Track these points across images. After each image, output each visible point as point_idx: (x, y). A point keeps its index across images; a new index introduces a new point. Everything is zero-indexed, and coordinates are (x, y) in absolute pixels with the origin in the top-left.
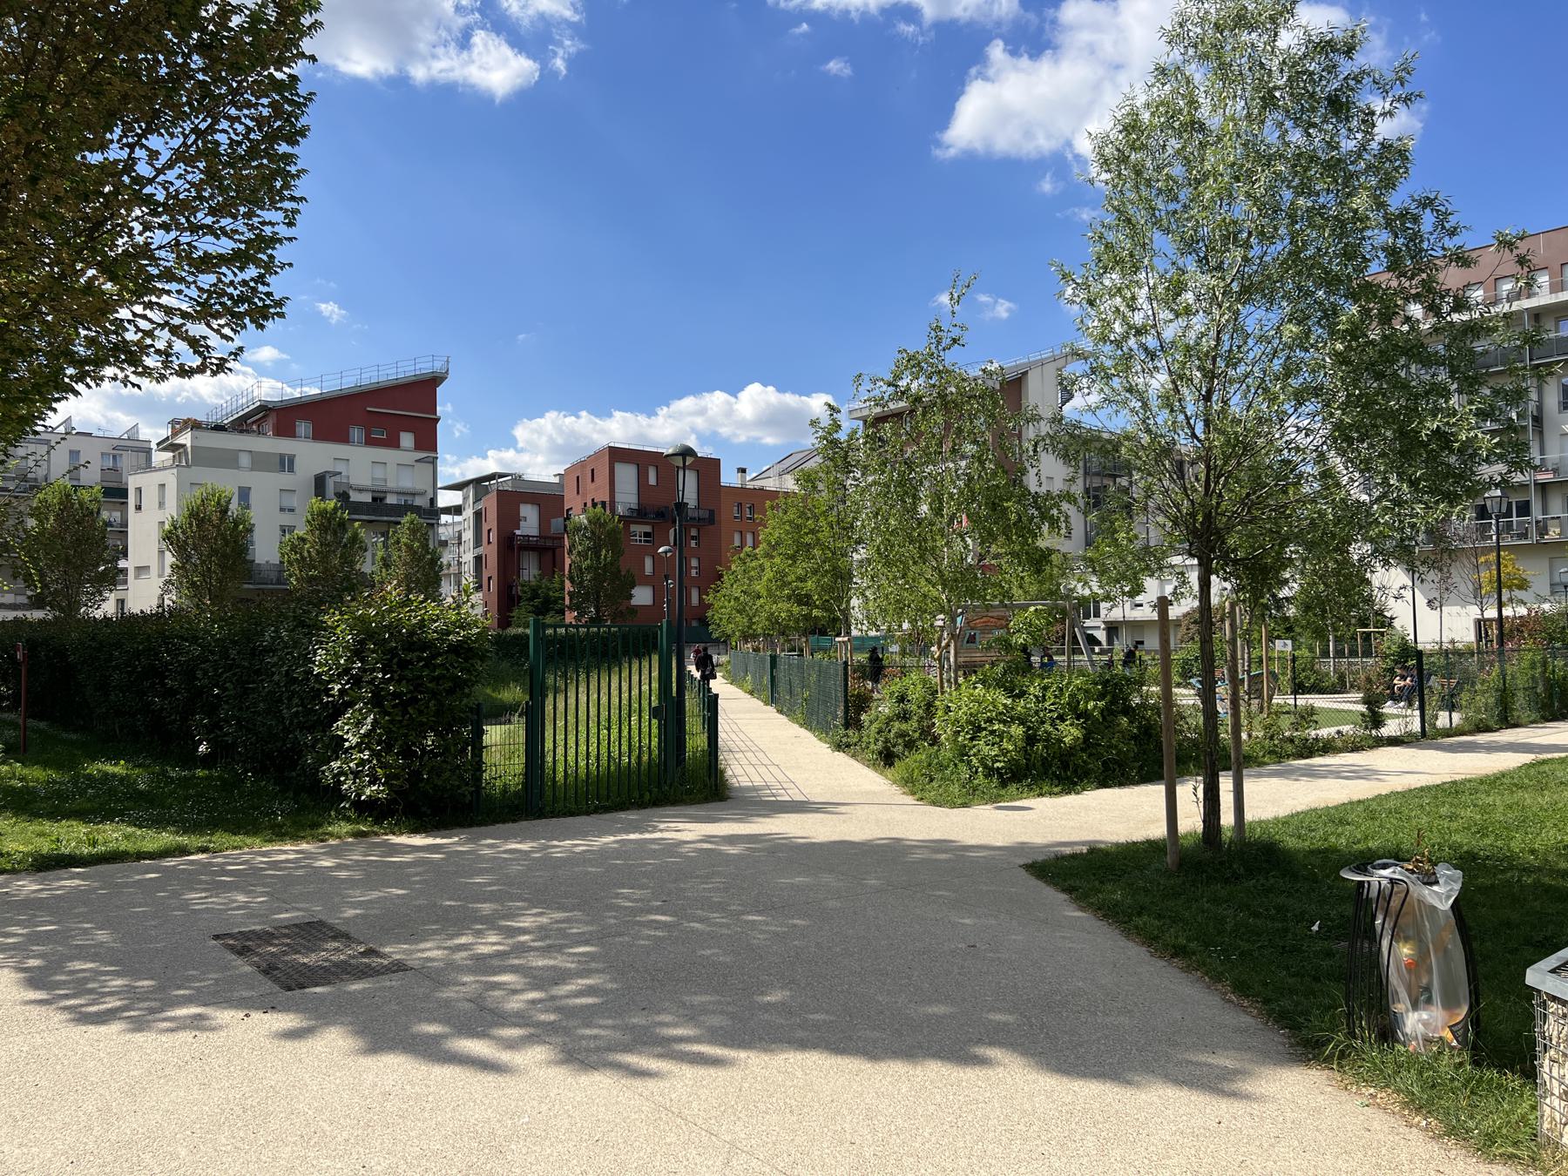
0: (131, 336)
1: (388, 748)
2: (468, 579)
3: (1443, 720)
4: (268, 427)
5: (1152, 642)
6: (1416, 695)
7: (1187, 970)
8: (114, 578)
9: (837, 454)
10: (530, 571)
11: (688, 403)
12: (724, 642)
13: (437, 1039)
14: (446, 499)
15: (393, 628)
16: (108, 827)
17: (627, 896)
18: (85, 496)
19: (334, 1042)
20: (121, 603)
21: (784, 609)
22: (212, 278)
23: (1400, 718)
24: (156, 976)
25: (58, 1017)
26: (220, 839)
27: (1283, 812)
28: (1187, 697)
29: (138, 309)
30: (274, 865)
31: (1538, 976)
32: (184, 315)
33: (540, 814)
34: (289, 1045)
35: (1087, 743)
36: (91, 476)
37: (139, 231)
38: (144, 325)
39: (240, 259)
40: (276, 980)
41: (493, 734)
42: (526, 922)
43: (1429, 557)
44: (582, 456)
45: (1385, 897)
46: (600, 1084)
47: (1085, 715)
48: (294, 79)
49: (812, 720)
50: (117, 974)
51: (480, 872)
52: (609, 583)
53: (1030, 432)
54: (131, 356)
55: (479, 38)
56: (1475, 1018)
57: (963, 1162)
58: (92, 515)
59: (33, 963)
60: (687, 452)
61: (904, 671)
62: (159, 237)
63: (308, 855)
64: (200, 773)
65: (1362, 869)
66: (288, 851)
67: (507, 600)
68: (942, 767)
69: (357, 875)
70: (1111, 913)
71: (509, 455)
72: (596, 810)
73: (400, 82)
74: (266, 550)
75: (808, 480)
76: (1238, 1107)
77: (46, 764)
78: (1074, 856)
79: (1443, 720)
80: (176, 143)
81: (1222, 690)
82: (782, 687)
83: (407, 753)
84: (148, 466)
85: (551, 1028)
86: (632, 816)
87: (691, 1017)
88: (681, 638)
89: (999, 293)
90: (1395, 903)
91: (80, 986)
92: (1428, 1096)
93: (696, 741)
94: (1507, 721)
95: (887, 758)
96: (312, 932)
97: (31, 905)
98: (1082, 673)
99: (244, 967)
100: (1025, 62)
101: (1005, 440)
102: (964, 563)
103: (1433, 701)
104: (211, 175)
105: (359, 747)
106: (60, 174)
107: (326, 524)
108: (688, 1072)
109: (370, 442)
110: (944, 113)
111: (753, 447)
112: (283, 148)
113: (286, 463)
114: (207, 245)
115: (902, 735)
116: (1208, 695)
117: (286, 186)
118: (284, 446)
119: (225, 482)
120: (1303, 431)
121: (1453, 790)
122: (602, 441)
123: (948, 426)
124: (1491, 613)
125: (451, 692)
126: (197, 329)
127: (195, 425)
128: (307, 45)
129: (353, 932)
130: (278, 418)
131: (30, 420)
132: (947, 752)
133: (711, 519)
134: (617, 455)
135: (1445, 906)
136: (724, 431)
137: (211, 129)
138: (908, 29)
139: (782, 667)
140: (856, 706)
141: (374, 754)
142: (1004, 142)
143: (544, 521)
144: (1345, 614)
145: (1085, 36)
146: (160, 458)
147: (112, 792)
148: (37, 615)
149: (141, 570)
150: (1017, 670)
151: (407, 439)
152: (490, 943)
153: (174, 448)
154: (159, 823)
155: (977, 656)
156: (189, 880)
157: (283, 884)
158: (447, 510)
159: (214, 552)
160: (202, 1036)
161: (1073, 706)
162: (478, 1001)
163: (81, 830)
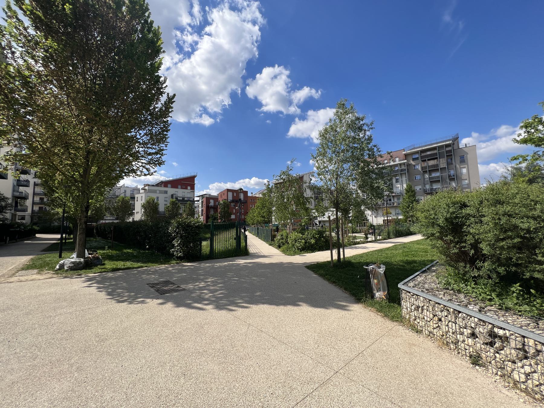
0: (135, 168)
1: (183, 246)
2: (200, 214)
3: (378, 238)
4: (163, 185)
5: (327, 224)
6: (373, 233)
7: (336, 286)
8: (132, 214)
9: (270, 190)
10: (212, 212)
11: (242, 181)
12: (248, 225)
13: (190, 303)
14: (196, 199)
15: (185, 223)
16: (127, 262)
17: (230, 274)
18: (127, 198)
19: (169, 305)
20: (133, 219)
21: (260, 219)
22: (151, 157)
23: (371, 238)
24: (132, 293)
25: (114, 302)
26: (150, 264)
27: (351, 255)
28: (333, 234)
29: (136, 163)
30: (160, 269)
31: (400, 286)
32: (145, 164)
33: (213, 258)
34: (161, 306)
35: (316, 243)
36: (128, 194)
37: (137, 148)
38: (138, 166)
39: (156, 153)
40: (159, 293)
41: (204, 243)
42: (209, 280)
43: (375, 209)
44: (222, 191)
45: (372, 271)
46: (223, 313)
47: (316, 238)
48: (168, 120)
49: (265, 240)
50: (127, 292)
51: (201, 270)
52: (226, 214)
53: (305, 185)
54: (134, 171)
55: (204, 115)
56: (388, 293)
57: (294, 326)
58: (128, 202)
59: (110, 290)
60: (241, 189)
61: (282, 230)
62: (141, 149)
63: (168, 268)
64: (147, 251)
65: (367, 266)
66: (163, 267)
67: (208, 217)
68: (289, 248)
69: (176, 271)
70: (321, 275)
71: (208, 190)
72: (224, 258)
73: (189, 123)
74: (161, 208)
75: (264, 195)
76: (346, 312)
77: (116, 250)
78: (314, 264)
79: (378, 238)
80: (145, 132)
81: (340, 233)
82: (260, 234)
83: (187, 247)
84: (139, 193)
85: (214, 301)
86: (230, 259)
87: (241, 299)
88: (240, 225)
89: (298, 162)
90: (373, 272)
91: (119, 295)
92: (381, 309)
93: (243, 244)
94: (389, 238)
95: (279, 247)
96: (167, 283)
97: (111, 279)
98: (315, 230)
99: (152, 290)
100: (302, 121)
101: (300, 187)
102: (291, 210)
103: (376, 234)
104: (151, 138)
105: (177, 246)
106: (122, 137)
107: (173, 203)
108: (241, 310)
109: (182, 188)
110: (288, 130)
111: (254, 189)
112: (165, 133)
113: (166, 192)
114: (150, 151)
115: (282, 242)
116: (337, 233)
117: (166, 140)
118: (165, 189)
119: (154, 196)
120: (353, 186)
121: (381, 251)
122: (226, 188)
123: (289, 185)
124: (386, 218)
125: (195, 235)
126: (148, 166)
127: (149, 185)
128: (170, 115)
129: (175, 282)
130: (165, 184)
131: (115, 184)
132: (290, 246)
133: (246, 202)
134: (228, 190)
135: (382, 272)
136: (248, 186)
137: (152, 129)
138: (281, 115)
139: (259, 230)
140: (274, 237)
141: (181, 247)
142: (299, 135)
143: (215, 203)
144: (361, 219)
145: (312, 117)
146: (141, 191)
147: (129, 255)
148: (116, 221)
149: (137, 213)
150: (303, 231)
151: (189, 188)
152: (202, 284)
153: (144, 189)
154: (138, 261)
155: (296, 227)
156: (143, 273)
157: (161, 273)
158: (196, 201)
159: (151, 209)
160: (143, 305)
161: (313, 236)
162: (199, 296)
163: (122, 263)
